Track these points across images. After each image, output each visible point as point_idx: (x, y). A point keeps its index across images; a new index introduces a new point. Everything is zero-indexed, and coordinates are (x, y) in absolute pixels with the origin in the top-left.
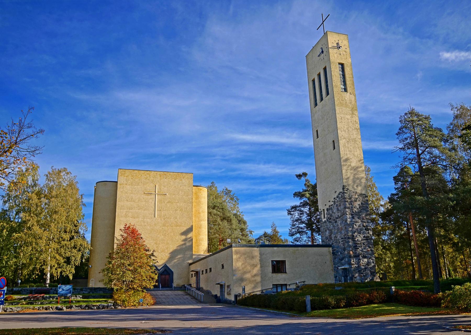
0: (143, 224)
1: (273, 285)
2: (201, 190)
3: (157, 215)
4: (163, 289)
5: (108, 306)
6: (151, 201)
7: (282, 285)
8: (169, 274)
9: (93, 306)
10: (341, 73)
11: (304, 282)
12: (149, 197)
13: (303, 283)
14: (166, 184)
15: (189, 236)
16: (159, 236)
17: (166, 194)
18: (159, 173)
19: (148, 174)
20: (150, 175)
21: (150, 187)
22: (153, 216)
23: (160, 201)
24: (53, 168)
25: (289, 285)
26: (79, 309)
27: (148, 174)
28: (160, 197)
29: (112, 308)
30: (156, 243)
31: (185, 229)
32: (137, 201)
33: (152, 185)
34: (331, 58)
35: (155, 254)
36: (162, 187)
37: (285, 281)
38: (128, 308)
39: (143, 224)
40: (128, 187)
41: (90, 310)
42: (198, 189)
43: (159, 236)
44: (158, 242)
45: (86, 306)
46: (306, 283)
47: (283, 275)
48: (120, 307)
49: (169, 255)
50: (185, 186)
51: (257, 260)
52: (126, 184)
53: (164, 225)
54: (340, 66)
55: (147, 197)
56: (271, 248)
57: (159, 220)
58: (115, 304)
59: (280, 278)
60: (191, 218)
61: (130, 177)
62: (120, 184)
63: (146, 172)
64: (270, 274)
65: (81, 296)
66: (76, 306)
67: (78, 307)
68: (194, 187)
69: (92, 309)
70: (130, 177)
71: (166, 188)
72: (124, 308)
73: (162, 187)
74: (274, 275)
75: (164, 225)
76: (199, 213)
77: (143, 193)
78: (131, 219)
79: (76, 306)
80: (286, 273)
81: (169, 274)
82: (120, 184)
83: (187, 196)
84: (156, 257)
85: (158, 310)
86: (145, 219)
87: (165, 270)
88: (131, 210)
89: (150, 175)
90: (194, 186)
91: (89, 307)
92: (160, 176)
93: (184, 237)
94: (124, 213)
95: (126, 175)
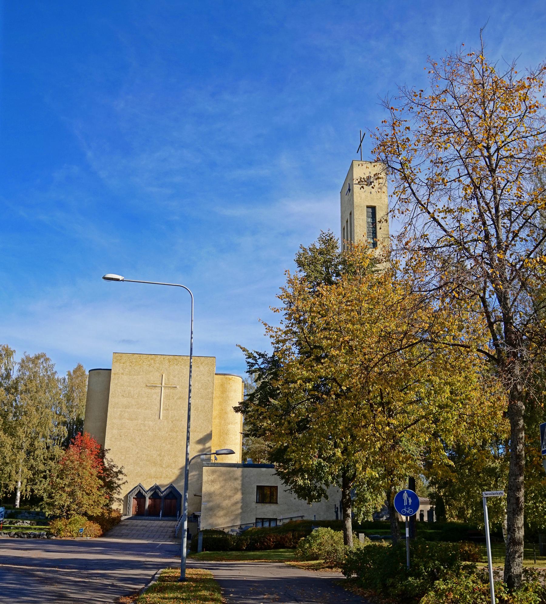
0: (142, 427)
1: (257, 519)
2: (230, 379)
3: (163, 416)
4: (163, 518)
5: (40, 535)
6: (154, 396)
7: (270, 520)
8: (176, 499)
9: (24, 534)
10: (370, 220)
11: (302, 517)
12: (153, 391)
13: (300, 519)
14: (176, 373)
15: (207, 445)
16: (164, 445)
17: (176, 387)
18: (168, 357)
19: (152, 359)
20: (155, 361)
21: (154, 378)
22: (157, 417)
23: (167, 396)
24: (26, 354)
25: (280, 520)
26: (7, 537)
27: (152, 359)
28: (167, 391)
29: (44, 538)
30: (160, 455)
31: (201, 436)
32: (136, 397)
33: (158, 375)
34: (355, 200)
35: (124, 471)
36: (172, 377)
37: (274, 514)
38: (63, 538)
39: (142, 427)
40: (125, 377)
41: (19, 539)
42: (226, 378)
43: (164, 445)
44: (163, 453)
45: (15, 534)
46: (305, 519)
47: (273, 507)
48: (54, 537)
49: (180, 471)
50: (203, 375)
51: (238, 484)
52: (122, 374)
53: (172, 430)
54: (370, 210)
55: (150, 391)
56: (258, 469)
57: (166, 423)
58: (49, 534)
59: (267, 510)
60: (210, 421)
61: (128, 364)
62: (115, 374)
63: (150, 357)
64: (254, 505)
65: (29, 522)
66: (4, 533)
67: (6, 534)
68: (217, 376)
69: (21, 537)
70: (128, 364)
71: (176, 379)
72: (59, 539)
73: (172, 377)
74: (260, 506)
75: (172, 430)
76: (226, 413)
77: (144, 385)
78: (127, 421)
79: (4, 533)
80: (277, 503)
81: (176, 499)
82: (115, 374)
83: (206, 389)
84: (125, 475)
85: (93, 543)
86: (146, 422)
87: (171, 492)
88: (127, 410)
89: (155, 361)
90: (216, 374)
91: (18, 535)
92: (169, 362)
93: (200, 447)
94: (119, 414)
95: (123, 361)
